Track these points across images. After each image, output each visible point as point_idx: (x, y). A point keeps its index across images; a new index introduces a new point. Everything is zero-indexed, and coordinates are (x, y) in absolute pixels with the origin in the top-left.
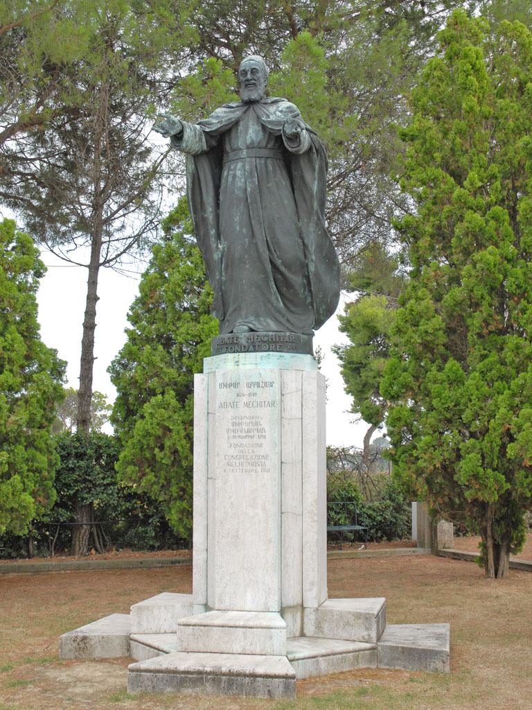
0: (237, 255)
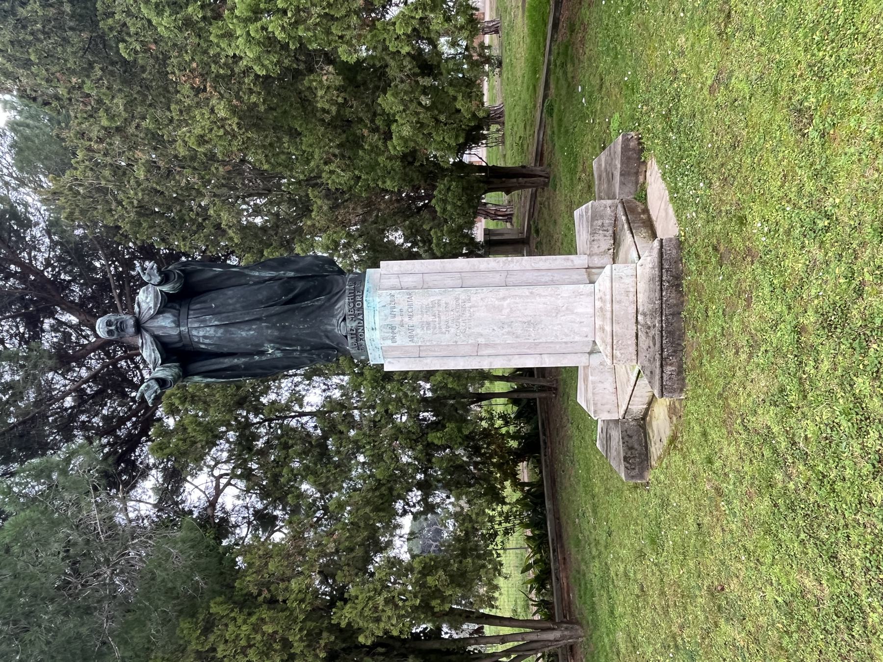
0: (276, 333)
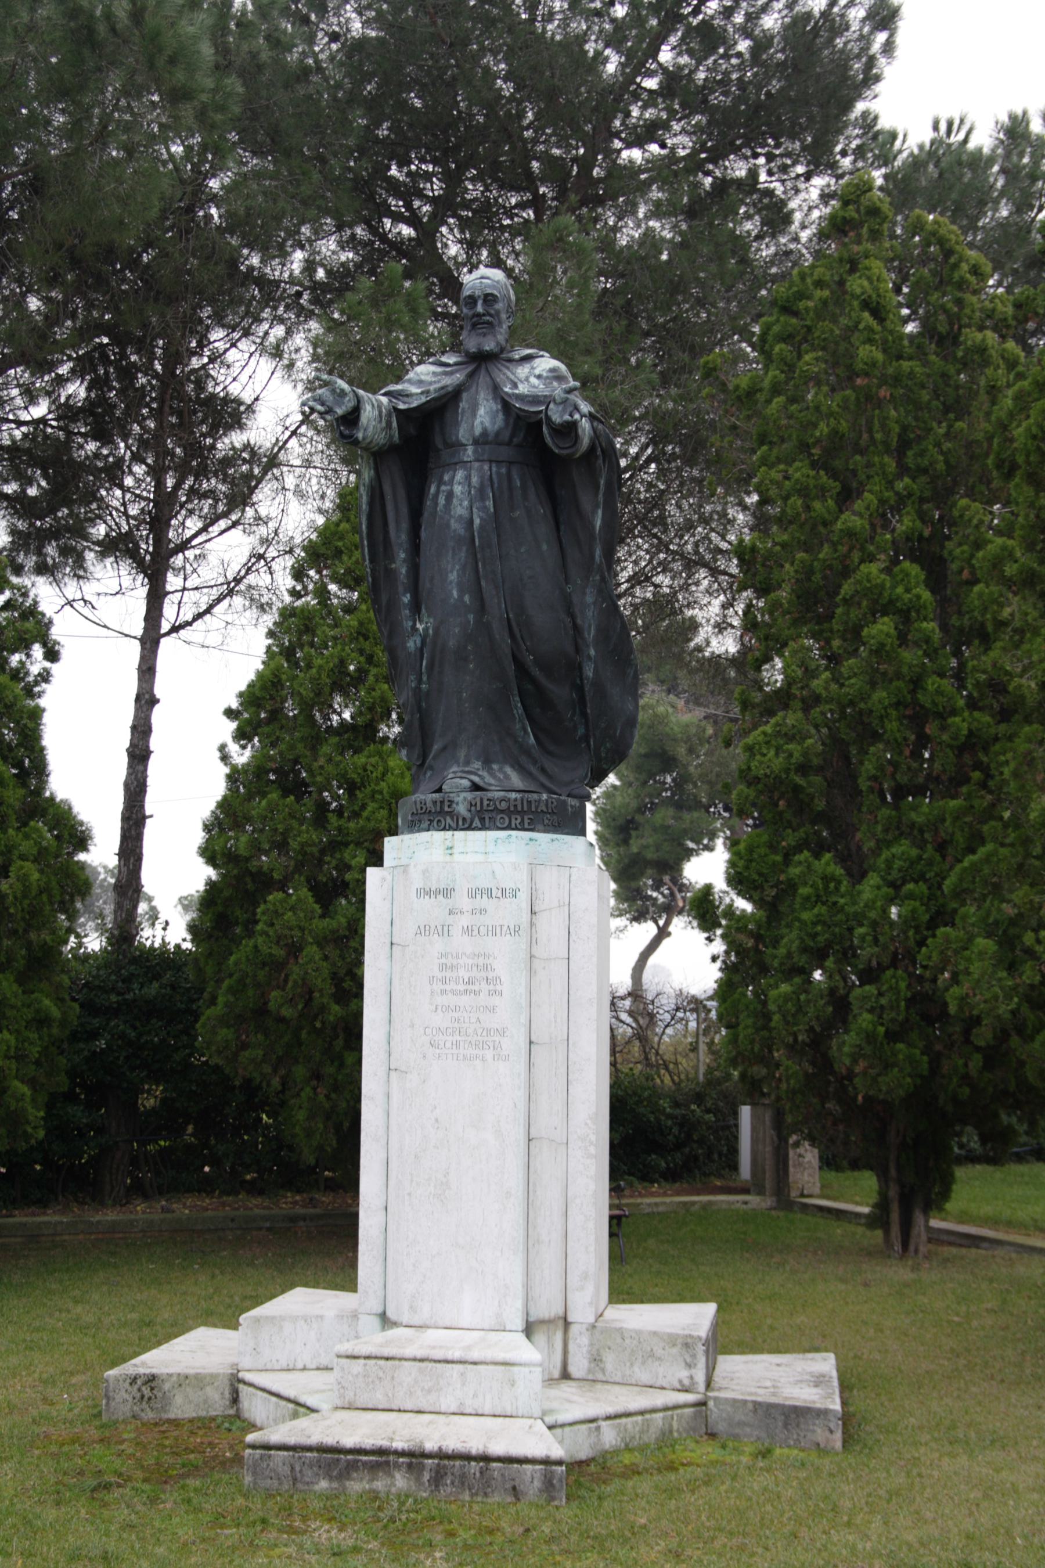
0: (452, 643)
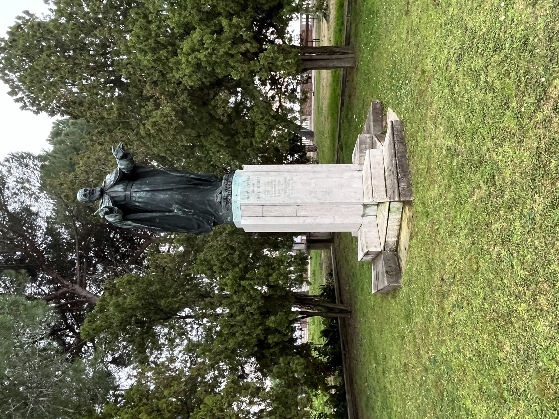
0: (181, 197)
